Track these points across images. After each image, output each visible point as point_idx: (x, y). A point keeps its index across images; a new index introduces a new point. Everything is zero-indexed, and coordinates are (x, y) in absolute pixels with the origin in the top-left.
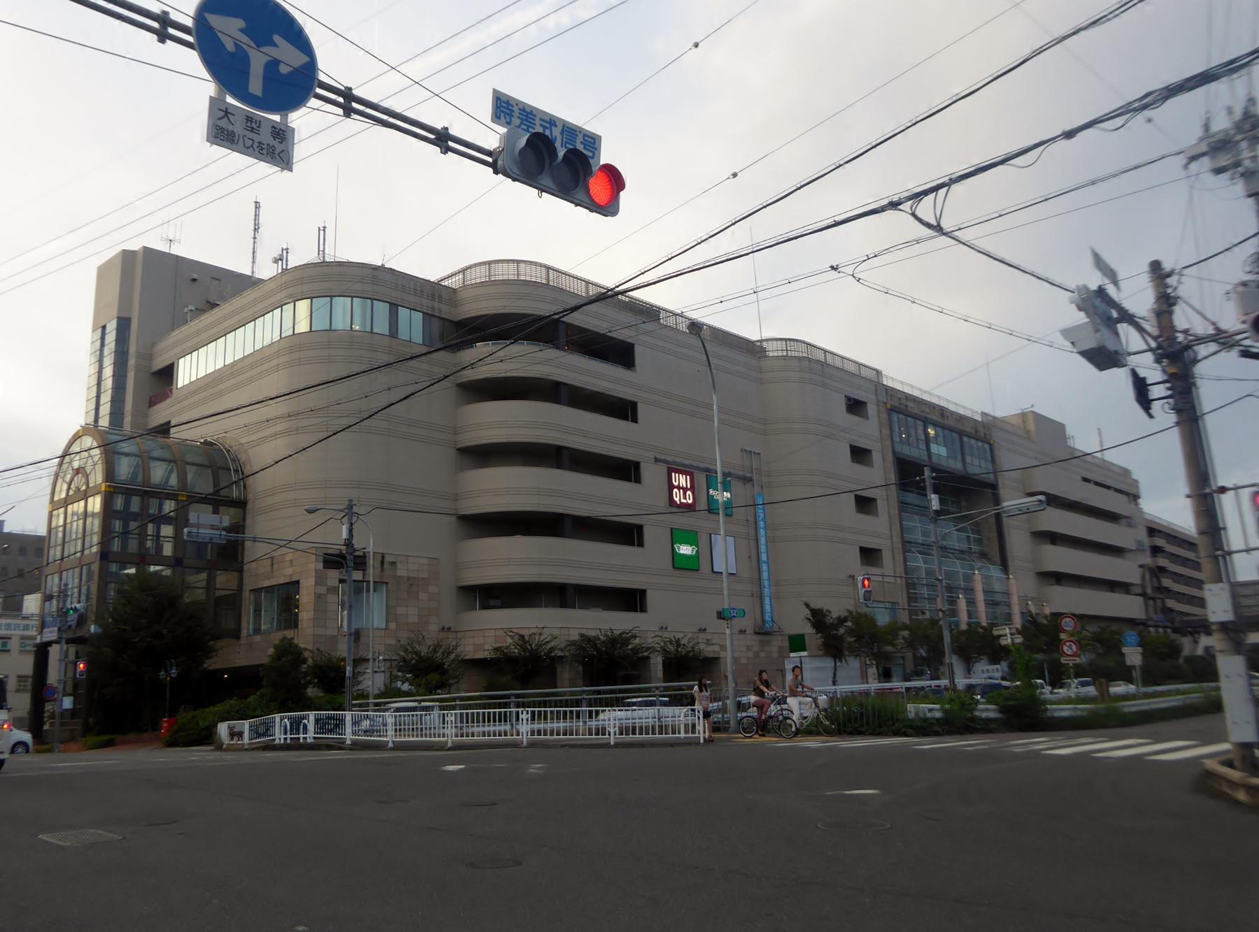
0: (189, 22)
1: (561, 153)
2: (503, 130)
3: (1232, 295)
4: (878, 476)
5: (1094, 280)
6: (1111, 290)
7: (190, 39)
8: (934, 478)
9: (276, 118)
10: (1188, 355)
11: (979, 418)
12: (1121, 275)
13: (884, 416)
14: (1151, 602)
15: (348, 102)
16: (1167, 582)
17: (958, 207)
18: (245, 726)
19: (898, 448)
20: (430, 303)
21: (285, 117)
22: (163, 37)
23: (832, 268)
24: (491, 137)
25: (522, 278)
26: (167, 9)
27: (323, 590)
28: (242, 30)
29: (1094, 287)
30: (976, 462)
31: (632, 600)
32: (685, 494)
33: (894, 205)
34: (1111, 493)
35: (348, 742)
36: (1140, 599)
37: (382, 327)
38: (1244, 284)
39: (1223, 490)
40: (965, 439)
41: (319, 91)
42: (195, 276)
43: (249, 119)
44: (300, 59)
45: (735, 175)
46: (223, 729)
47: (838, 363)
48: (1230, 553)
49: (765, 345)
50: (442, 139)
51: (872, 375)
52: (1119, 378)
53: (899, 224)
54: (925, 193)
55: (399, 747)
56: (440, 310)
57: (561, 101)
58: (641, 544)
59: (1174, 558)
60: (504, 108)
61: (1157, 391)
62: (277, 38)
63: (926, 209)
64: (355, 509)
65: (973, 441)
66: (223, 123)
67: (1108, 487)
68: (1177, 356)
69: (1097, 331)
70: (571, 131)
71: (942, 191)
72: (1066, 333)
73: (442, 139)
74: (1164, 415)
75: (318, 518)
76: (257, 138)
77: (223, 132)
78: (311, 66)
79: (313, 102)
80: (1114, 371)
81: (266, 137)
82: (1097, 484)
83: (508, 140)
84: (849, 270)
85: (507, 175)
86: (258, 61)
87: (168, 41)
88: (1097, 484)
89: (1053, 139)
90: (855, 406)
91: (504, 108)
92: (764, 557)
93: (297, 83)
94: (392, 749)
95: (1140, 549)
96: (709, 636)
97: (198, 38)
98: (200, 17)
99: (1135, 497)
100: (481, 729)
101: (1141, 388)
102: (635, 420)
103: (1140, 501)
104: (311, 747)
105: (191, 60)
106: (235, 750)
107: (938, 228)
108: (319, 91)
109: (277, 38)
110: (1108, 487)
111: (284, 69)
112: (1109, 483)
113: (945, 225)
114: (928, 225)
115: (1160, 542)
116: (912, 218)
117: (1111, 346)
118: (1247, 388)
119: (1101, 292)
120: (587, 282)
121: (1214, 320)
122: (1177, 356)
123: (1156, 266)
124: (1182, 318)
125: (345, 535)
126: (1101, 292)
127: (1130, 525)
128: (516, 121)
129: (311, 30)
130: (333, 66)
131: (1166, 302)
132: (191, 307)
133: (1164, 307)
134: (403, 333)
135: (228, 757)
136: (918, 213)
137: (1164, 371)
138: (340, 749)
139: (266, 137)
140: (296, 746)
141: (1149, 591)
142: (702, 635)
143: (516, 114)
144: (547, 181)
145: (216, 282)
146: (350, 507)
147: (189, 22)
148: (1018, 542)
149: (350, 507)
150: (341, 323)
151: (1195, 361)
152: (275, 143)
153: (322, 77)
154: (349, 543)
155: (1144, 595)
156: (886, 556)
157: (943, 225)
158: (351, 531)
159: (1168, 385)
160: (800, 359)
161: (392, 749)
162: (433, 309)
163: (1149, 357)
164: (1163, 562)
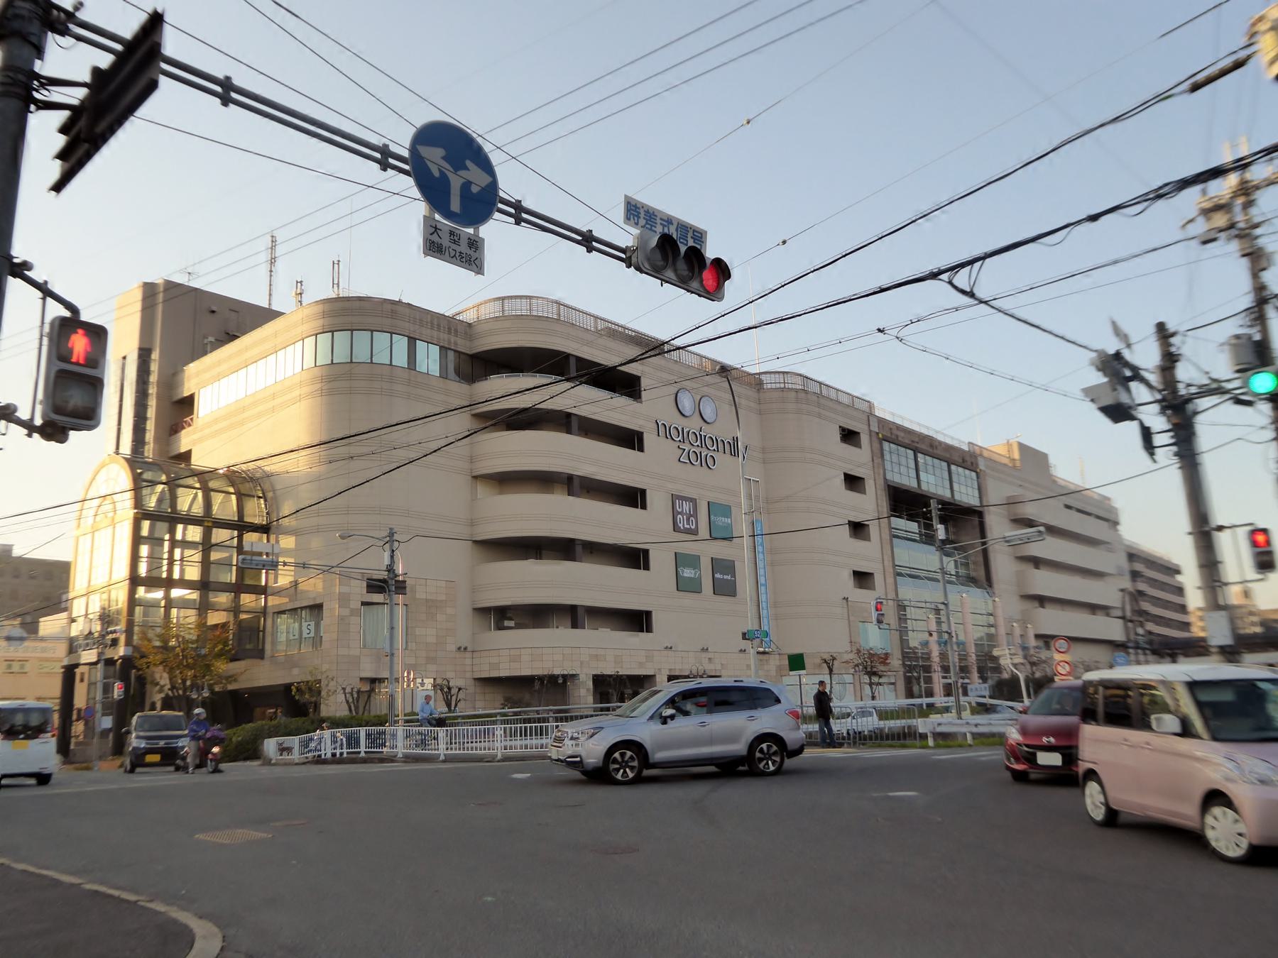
0: (406, 154)
1: (683, 249)
2: (636, 231)
3: (1226, 348)
4: (869, 505)
5: (1112, 346)
6: (1127, 355)
7: (407, 167)
8: (939, 510)
9: (471, 231)
10: (1190, 407)
11: (966, 448)
12: (1133, 340)
13: (876, 445)
14: (1130, 624)
15: (519, 213)
16: (1146, 606)
17: (989, 279)
18: (294, 741)
19: (889, 477)
20: (446, 336)
21: (477, 229)
22: (385, 166)
23: (879, 330)
24: (626, 236)
25: (535, 313)
26: (387, 142)
27: (346, 612)
28: (443, 158)
29: (1112, 351)
30: (963, 489)
31: (638, 621)
32: (688, 519)
33: (934, 275)
34: (1092, 519)
35: (400, 755)
36: (1121, 621)
37: (401, 359)
38: (1237, 337)
39: (1220, 528)
40: (953, 467)
41: (500, 206)
42: (214, 308)
43: (452, 233)
44: (484, 180)
45: (784, 242)
46: (270, 746)
47: (833, 394)
48: (1226, 584)
49: (763, 377)
50: (588, 241)
51: (865, 407)
52: (1130, 430)
53: (937, 288)
54: (962, 265)
55: (448, 759)
56: (456, 344)
57: (679, 205)
58: (647, 567)
59: (1153, 582)
60: (634, 211)
61: (1158, 440)
62: (468, 163)
63: (962, 279)
64: (396, 537)
65: (960, 470)
66: (435, 238)
67: (1089, 514)
68: (1180, 410)
69: (1115, 390)
70: (684, 228)
71: (979, 264)
72: (1087, 391)
73: (588, 241)
74: (1166, 455)
75: (355, 545)
76: (458, 249)
77: (433, 247)
78: (493, 186)
79: (497, 215)
80: (1127, 423)
81: (464, 248)
82: (1079, 511)
83: (642, 240)
84: (894, 332)
85: (639, 269)
86: (456, 182)
87: (231, 105)
88: (1079, 511)
89: (1079, 222)
90: (849, 436)
91: (634, 211)
92: (762, 580)
93: (483, 202)
94: (444, 761)
95: (1121, 574)
96: (711, 655)
97: (413, 168)
98: (413, 149)
99: (1115, 523)
100: (524, 742)
101: (1147, 434)
102: (641, 449)
103: (1119, 527)
104: (364, 761)
105: (408, 184)
106: (286, 764)
107: (971, 294)
108: (500, 206)
109: (468, 163)
110: (1089, 514)
111: (475, 189)
112: (1088, 509)
113: (979, 293)
114: (963, 292)
115: (1139, 567)
116: (949, 286)
117: (1124, 398)
118: (1238, 432)
119: (1118, 356)
120: (596, 318)
121: (1207, 369)
122: (1180, 410)
123: (1161, 327)
124: (1183, 373)
125: (387, 561)
126: (1118, 356)
127: (1110, 551)
128: (642, 222)
129: (495, 158)
130: (510, 184)
131: (1170, 360)
132: (211, 339)
133: (1168, 364)
134: (422, 366)
135: (277, 770)
136: (955, 282)
137: (1169, 421)
138: (392, 761)
139: (464, 248)
140: (353, 760)
141: (1128, 614)
142: (704, 655)
143: (642, 215)
144: (670, 274)
145: (233, 314)
146: (391, 534)
147: (406, 154)
148: (1003, 565)
149: (391, 534)
150: (362, 355)
151: (1196, 413)
152: (471, 252)
153: (502, 194)
154: (390, 569)
155: (1123, 618)
156: (878, 579)
157: (975, 291)
158: (392, 557)
159: (1171, 434)
160: (797, 391)
161: (444, 761)
162: (449, 342)
163: (1155, 408)
164: (1142, 586)
